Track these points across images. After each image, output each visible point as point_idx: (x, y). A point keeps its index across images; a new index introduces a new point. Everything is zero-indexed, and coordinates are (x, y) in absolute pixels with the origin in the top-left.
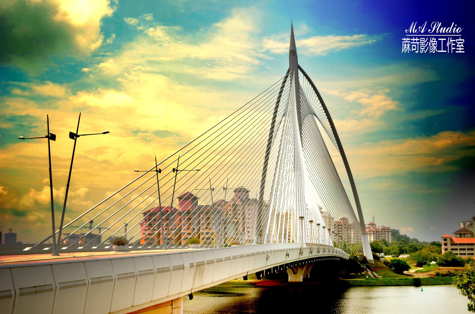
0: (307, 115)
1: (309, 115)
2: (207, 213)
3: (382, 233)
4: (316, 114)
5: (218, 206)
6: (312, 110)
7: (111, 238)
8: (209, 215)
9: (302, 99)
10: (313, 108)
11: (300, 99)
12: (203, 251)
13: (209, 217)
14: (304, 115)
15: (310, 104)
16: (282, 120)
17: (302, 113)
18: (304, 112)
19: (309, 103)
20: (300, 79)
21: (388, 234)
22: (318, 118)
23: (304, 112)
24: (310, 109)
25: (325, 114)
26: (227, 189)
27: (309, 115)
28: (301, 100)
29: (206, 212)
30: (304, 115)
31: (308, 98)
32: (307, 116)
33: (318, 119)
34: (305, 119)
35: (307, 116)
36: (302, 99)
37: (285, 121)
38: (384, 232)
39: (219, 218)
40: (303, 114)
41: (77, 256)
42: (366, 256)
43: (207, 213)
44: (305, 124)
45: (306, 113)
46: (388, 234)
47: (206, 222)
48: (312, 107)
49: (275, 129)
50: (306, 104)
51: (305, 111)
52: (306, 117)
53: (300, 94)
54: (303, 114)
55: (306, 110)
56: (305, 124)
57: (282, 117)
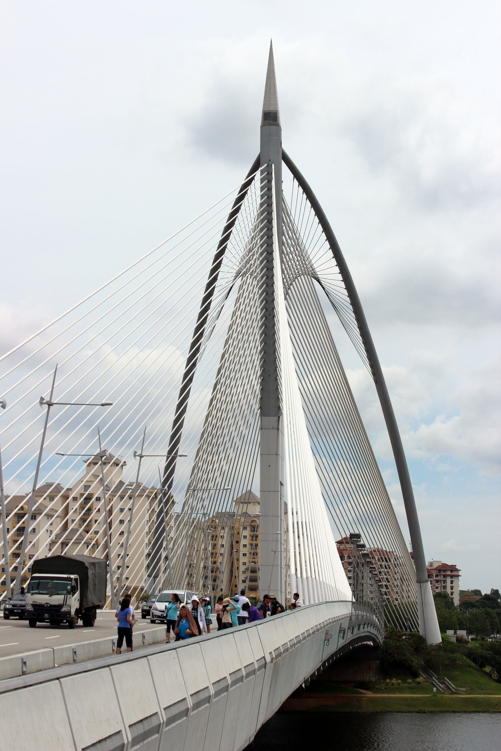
0: (296, 278)
1: (302, 277)
2: (19, 516)
3: (437, 578)
4: (319, 276)
5: (48, 499)
6: (309, 266)
7: (354, 615)
8: (23, 523)
9: (287, 237)
10: (313, 262)
11: (283, 237)
12: (234, 633)
13: (23, 526)
14: (289, 277)
15: (305, 251)
16: (231, 288)
17: (293, 270)
18: (290, 270)
19: (302, 248)
20: (284, 186)
21: (452, 582)
22: (324, 286)
23: (290, 270)
24: (305, 264)
25: (340, 277)
26: (143, 457)
27: (302, 277)
28: (285, 240)
29: (16, 514)
30: (289, 277)
31: (302, 235)
32: (296, 280)
33: (324, 288)
34: (292, 287)
35: (296, 280)
36: (287, 237)
37: (241, 287)
38: (442, 576)
39: (47, 530)
40: (288, 273)
41: (414, 714)
42: (424, 637)
43: (19, 516)
44: (291, 300)
45: (294, 271)
46: (452, 582)
47: (16, 538)
48: (311, 257)
49: (212, 313)
50: (297, 249)
51: (293, 267)
52: (294, 283)
53: (283, 225)
54: (288, 273)
55: (294, 261)
56: (291, 300)
57: (233, 278)
